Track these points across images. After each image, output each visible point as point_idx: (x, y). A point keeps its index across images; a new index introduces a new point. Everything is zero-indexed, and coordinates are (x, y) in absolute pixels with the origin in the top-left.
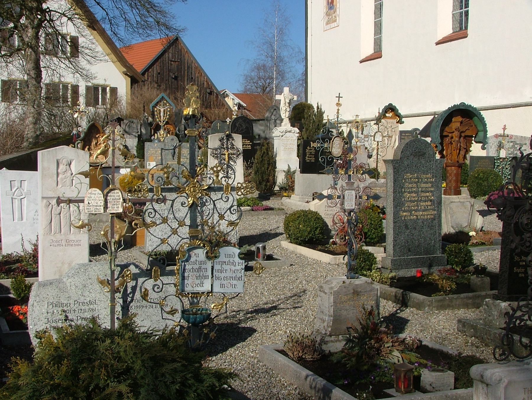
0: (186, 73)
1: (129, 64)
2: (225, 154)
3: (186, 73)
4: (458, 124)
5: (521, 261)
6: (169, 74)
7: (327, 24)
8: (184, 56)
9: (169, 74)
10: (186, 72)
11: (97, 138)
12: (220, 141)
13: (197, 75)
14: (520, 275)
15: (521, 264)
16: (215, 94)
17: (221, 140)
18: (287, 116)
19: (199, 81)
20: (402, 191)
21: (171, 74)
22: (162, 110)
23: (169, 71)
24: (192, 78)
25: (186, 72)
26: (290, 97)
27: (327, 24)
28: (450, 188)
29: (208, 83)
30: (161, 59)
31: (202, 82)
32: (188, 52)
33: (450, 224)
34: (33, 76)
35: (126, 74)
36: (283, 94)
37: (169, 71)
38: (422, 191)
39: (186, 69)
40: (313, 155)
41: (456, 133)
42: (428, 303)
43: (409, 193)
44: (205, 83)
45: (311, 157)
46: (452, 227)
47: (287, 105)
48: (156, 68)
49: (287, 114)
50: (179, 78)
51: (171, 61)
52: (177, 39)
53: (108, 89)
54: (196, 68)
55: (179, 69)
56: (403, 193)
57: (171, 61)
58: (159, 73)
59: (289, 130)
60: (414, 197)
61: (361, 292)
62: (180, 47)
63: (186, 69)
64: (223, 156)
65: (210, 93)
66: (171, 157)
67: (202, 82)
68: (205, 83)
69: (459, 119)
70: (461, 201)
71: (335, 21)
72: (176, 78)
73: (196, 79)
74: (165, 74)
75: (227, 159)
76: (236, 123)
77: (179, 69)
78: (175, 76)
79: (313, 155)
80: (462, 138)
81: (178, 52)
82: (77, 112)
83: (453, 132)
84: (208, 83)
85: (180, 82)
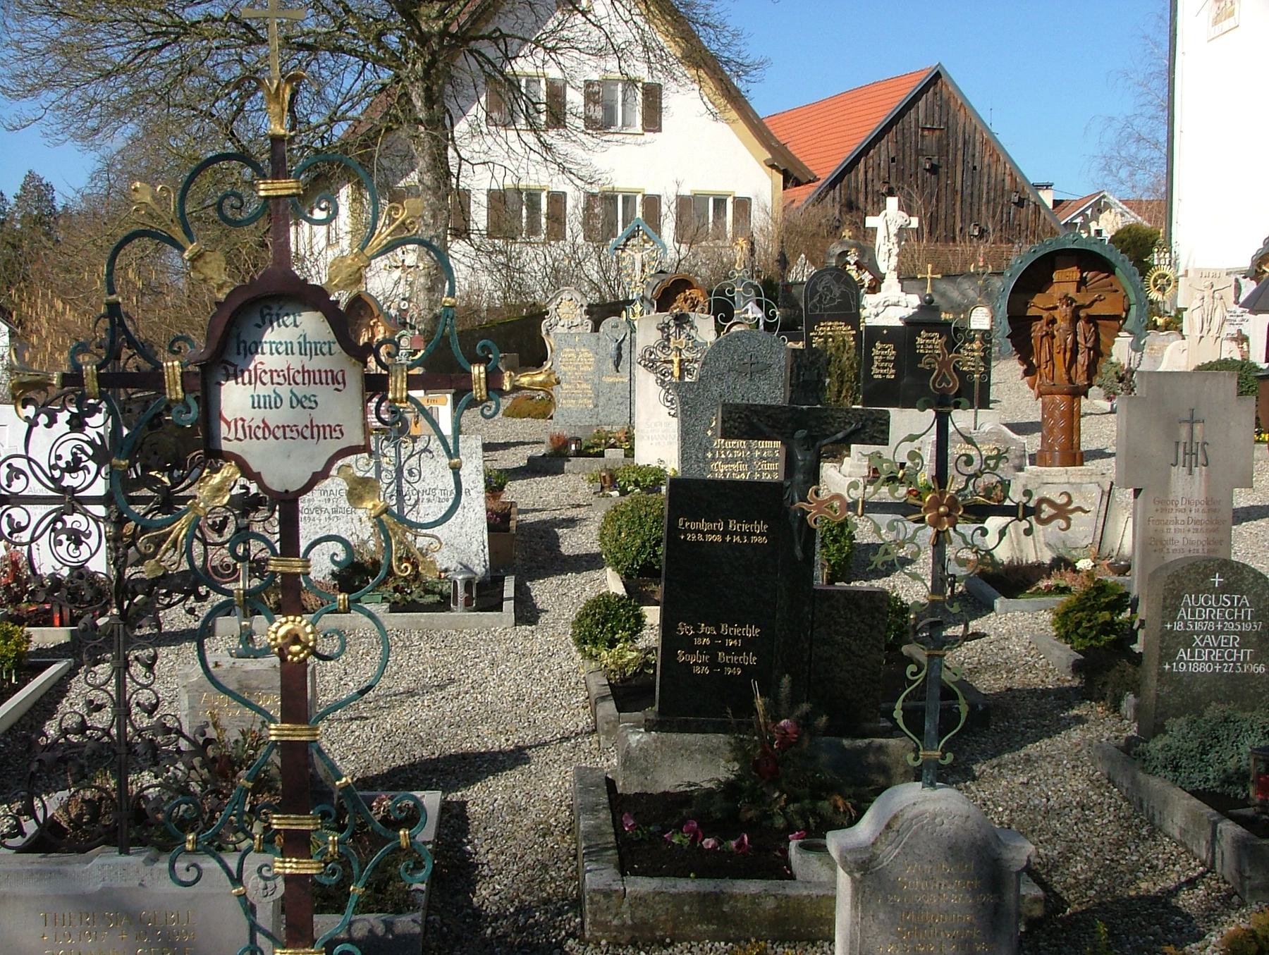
0: (960, 157)
1: (778, 142)
2: (672, 362)
3: (960, 157)
4: (1071, 290)
5: (696, 635)
6: (917, 160)
7: (1215, 23)
8: (955, 116)
9: (917, 160)
10: (960, 153)
11: (372, 328)
12: (662, 330)
13: (986, 161)
14: (697, 670)
15: (697, 641)
16: (1032, 206)
17: (664, 328)
18: (892, 267)
19: (993, 175)
20: (705, 457)
21: (922, 160)
22: (638, 257)
23: (919, 152)
24: (975, 168)
25: (960, 153)
26: (901, 222)
27: (1215, 23)
28: (1051, 447)
29: (1014, 180)
30: (899, 125)
31: (999, 178)
32: (965, 105)
33: (1042, 539)
34: (429, 183)
35: (772, 166)
36: (883, 213)
37: (919, 152)
38: (761, 458)
39: (960, 146)
40: (890, 361)
41: (1063, 311)
42: (606, 727)
43: (726, 461)
44: (1008, 179)
45: (884, 368)
46: (1048, 545)
47: (893, 239)
48: (886, 148)
49: (894, 261)
50: (943, 170)
51: (923, 129)
52: (938, 75)
53: (729, 201)
54: (985, 143)
55: (943, 149)
56: (709, 463)
57: (923, 129)
58: (893, 160)
59: (894, 300)
60: (771, 472)
61: (257, 688)
62: (945, 96)
63: (960, 146)
64: (669, 366)
65: (1020, 203)
66: (611, 366)
67: (999, 178)
68: (1008, 179)
69: (1074, 273)
70: (1072, 480)
71: (1231, 14)
72: (934, 170)
73: (985, 170)
74: (907, 160)
75: (677, 374)
76: (815, 284)
77: (943, 149)
78: (932, 165)
79: (890, 361)
80: (1081, 324)
81: (941, 107)
82: (397, 267)
83: (1056, 308)
84: (1014, 180)
85: (943, 178)
